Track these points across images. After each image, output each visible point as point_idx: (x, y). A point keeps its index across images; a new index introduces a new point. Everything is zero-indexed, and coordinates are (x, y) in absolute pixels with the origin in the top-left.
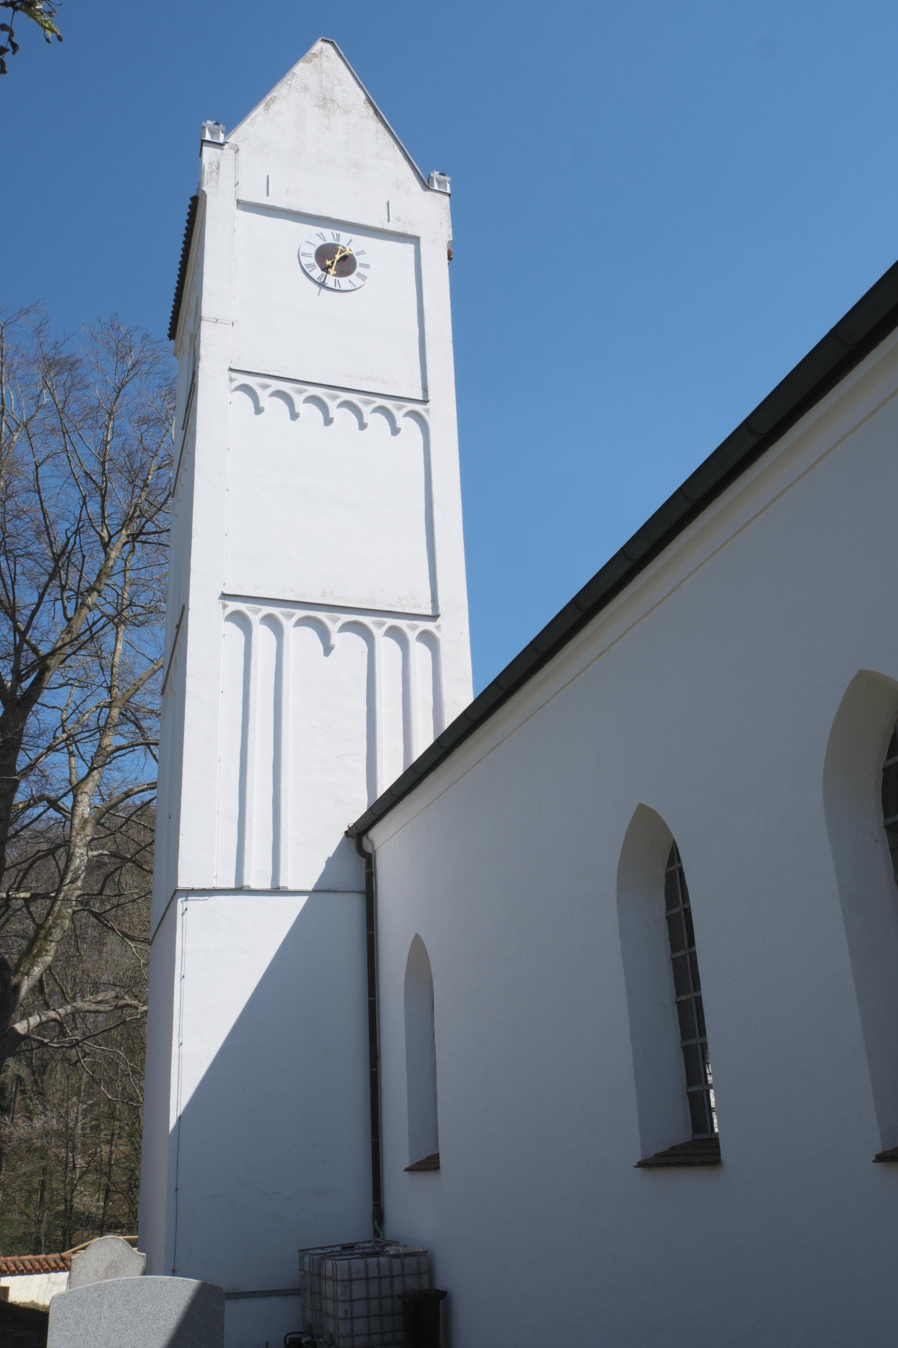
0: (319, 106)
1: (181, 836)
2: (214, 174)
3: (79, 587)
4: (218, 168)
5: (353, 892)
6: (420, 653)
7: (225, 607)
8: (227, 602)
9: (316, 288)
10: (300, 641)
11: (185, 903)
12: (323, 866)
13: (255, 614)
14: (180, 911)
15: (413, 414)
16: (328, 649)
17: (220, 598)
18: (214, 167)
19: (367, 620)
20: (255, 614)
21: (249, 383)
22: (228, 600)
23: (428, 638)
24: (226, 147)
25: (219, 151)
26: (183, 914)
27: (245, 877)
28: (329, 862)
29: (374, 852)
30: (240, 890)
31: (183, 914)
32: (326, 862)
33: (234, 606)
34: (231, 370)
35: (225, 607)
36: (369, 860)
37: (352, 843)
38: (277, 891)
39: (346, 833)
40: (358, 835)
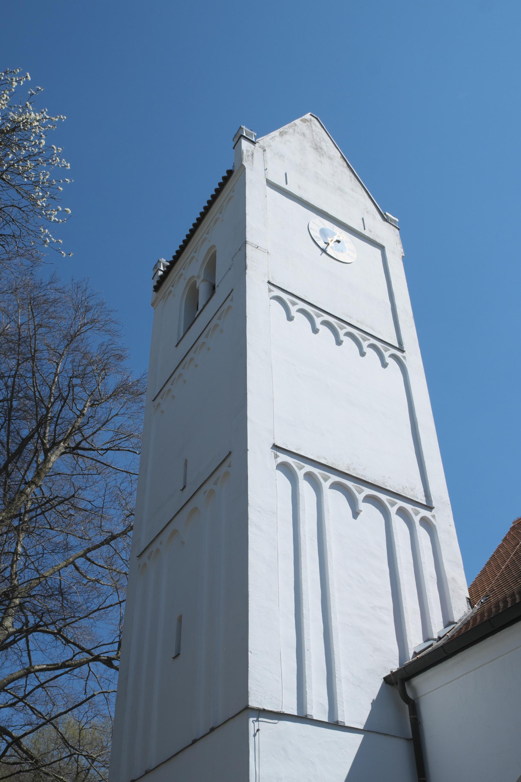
0: (314, 148)
1: (249, 654)
2: (250, 158)
3: (62, 407)
4: (252, 155)
5: (401, 738)
6: (422, 533)
7: (276, 457)
8: (278, 454)
9: (320, 251)
10: (335, 502)
11: (256, 723)
12: (369, 708)
13: (302, 470)
14: (251, 732)
15: (393, 356)
16: (356, 514)
17: (272, 448)
18: (250, 153)
19: (384, 497)
20: (302, 470)
21: (284, 298)
22: (278, 451)
23: (425, 522)
24: (257, 145)
25: (252, 146)
26: (255, 735)
27: (23, 739)
28: (374, 704)
29: (418, 698)
30: (303, 718)
31: (255, 735)
32: (372, 704)
33: (283, 458)
34: (269, 282)
35: (276, 457)
36: (414, 707)
37: (396, 691)
38: (334, 725)
39: (386, 679)
40: (400, 684)
